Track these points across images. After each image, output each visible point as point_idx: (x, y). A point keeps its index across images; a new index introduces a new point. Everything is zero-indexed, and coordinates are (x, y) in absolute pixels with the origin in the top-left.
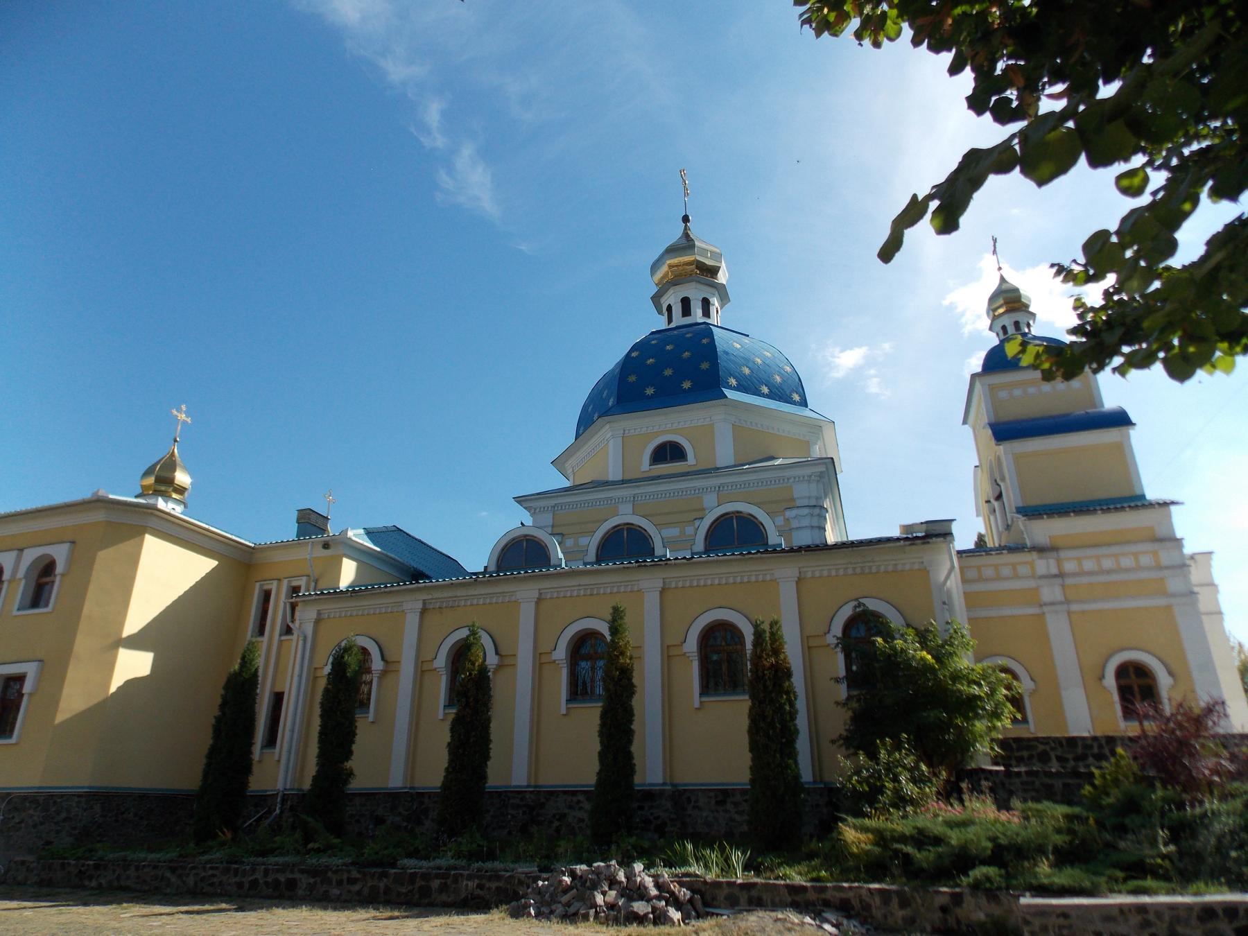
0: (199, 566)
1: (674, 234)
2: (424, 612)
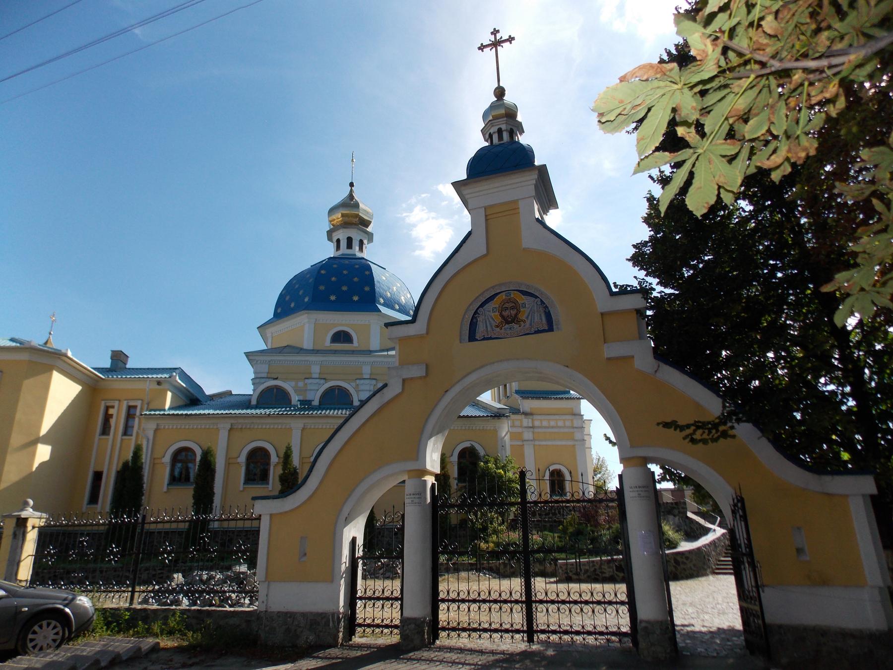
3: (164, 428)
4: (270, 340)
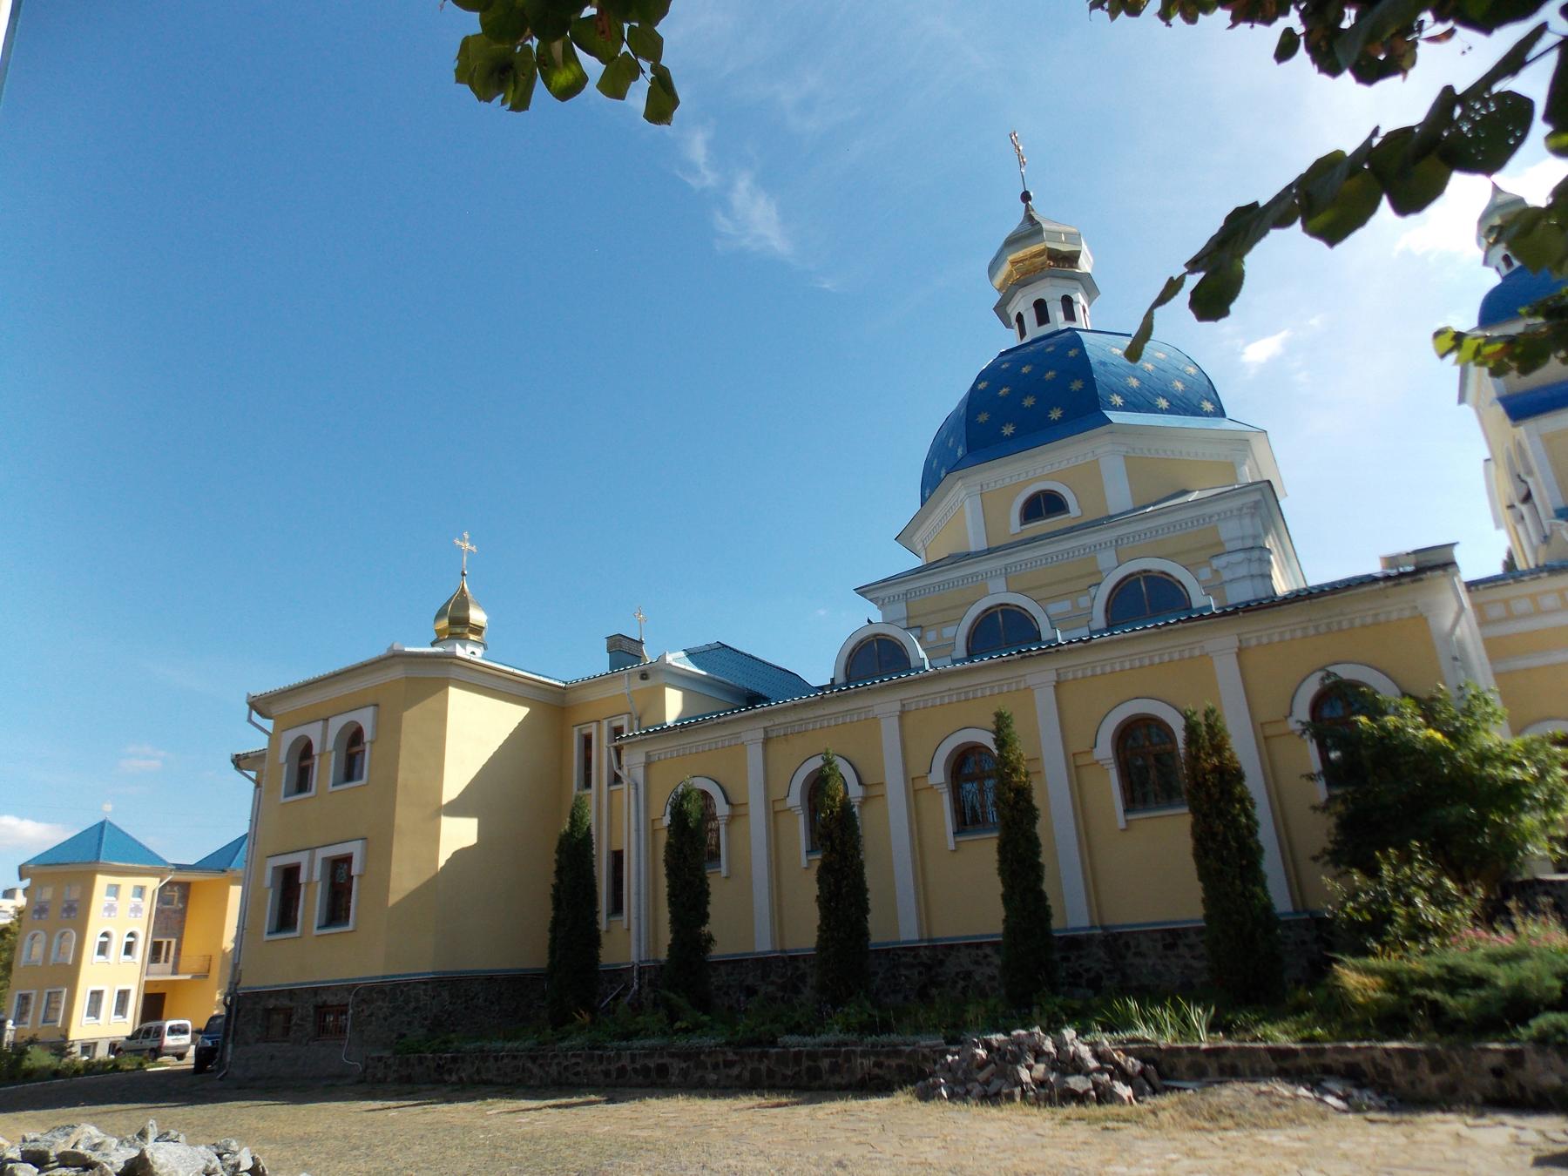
0: (511, 716)
1: (1014, 220)
2: (767, 741)
4: (923, 555)
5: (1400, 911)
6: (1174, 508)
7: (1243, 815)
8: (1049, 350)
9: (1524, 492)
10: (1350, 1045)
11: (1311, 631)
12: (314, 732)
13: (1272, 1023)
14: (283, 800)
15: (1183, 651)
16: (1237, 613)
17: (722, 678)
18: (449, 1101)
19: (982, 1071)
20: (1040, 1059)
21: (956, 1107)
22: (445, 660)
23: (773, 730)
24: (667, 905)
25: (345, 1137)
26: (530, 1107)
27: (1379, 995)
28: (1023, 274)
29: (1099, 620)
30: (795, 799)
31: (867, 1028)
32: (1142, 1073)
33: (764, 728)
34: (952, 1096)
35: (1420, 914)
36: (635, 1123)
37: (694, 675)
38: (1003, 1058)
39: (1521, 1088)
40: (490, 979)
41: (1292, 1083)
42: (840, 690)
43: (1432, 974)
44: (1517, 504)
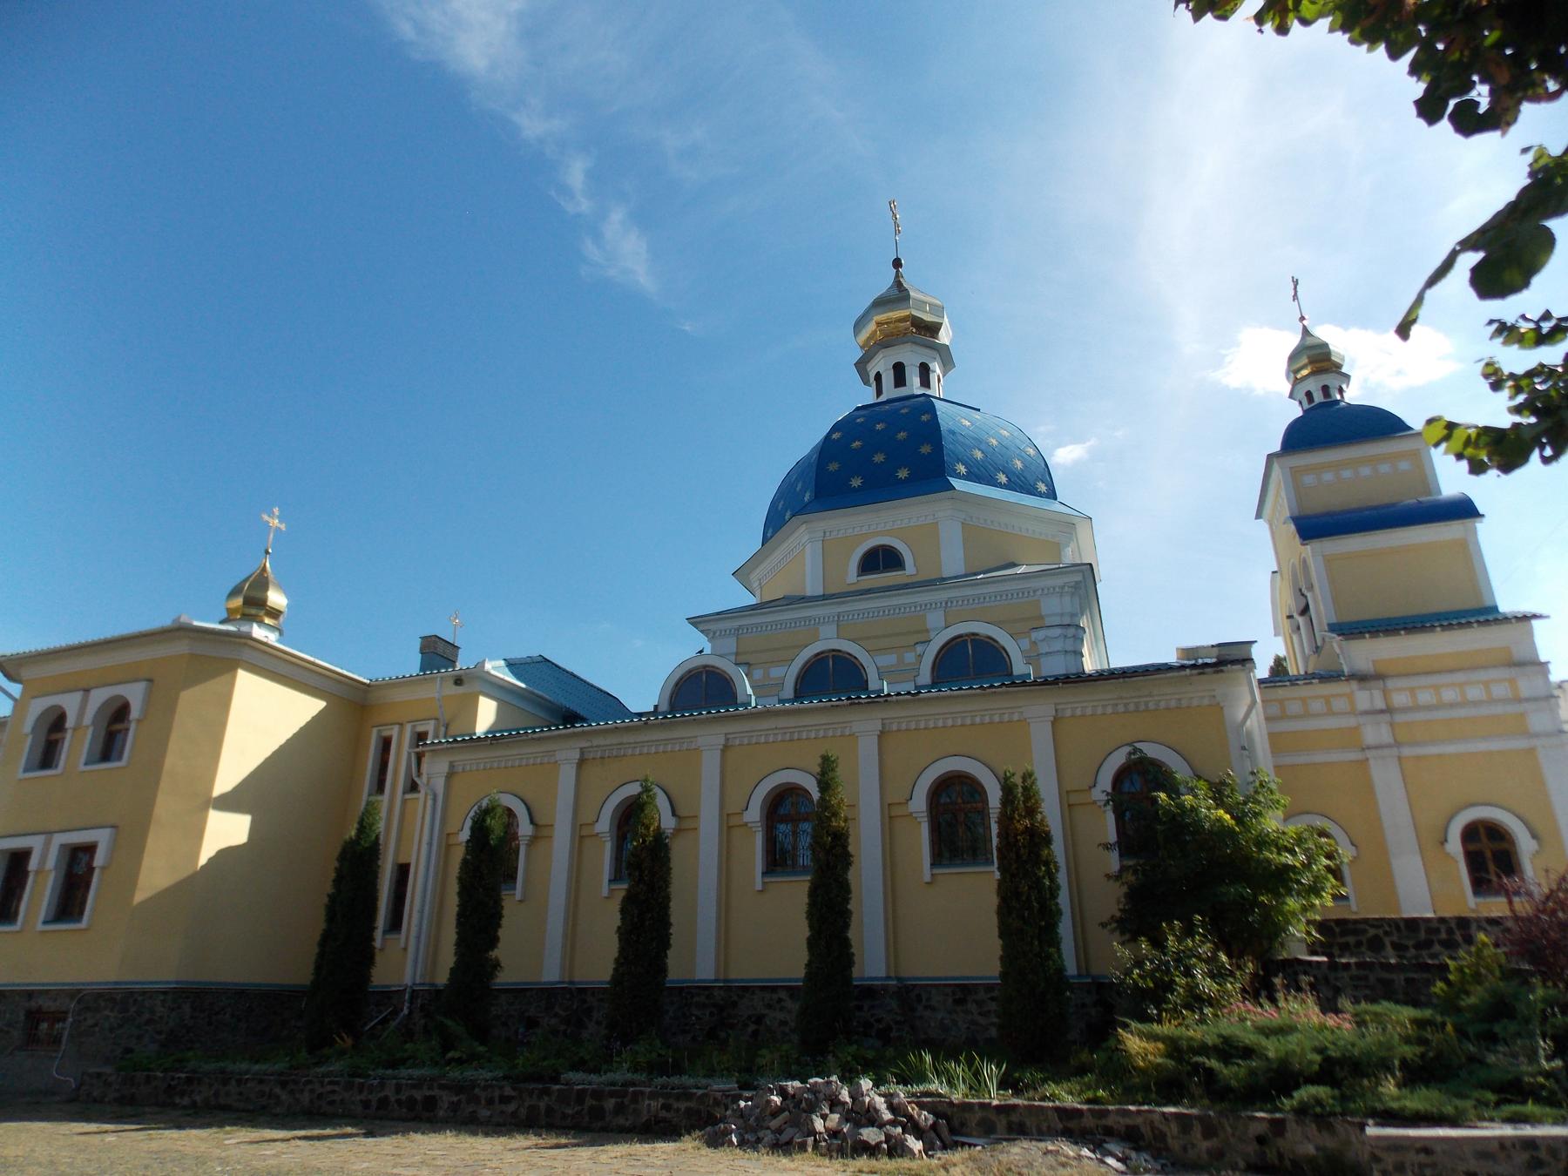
0: (303, 708)
1: (883, 283)
2: (581, 762)
3: (464, 771)
4: (758, 593)
5: (1179, 980)
6: (999, 578)
7: (1047, 877)
8: (903, 411)
9: (1302, 606)
10: (1132, 1108)
11: (1121, 708)
12: (70, 703)
13: (1057, 1083)
14: (21, 775)
15: (1004, 714)
16: (1057, 684)
17: (540, 693)
18: (180, 1127)
19: (775, 1118)
20: (835, 1108)
21: (747, 1155)
22: (238, 640)
23: (590, 752)
24: (455, 925)
25: (52, 1163)
26: (276, 1137)
27: (1159, 1060)
28: (887, 336)
29: (925, 677)
30: (604, 825)
31: (658, 1068)
32: (934, 1127)
33: (581, 749)
34: (742, 1144)
35: (1198, 984)
36: (398, 1160)
37: (505, 684)
38: (798, 1105)
39: (1281, 1156)
40: (240, 994)
41: (1076, 1143)
42: (665, 717)
43: (1210, 1043)
44: (1295, 615)
